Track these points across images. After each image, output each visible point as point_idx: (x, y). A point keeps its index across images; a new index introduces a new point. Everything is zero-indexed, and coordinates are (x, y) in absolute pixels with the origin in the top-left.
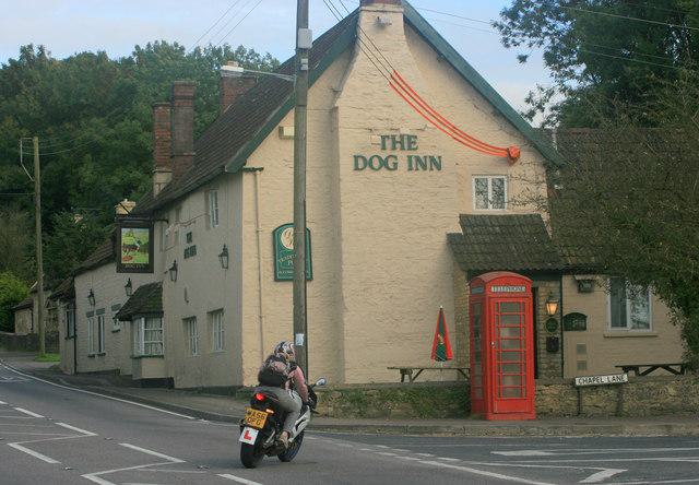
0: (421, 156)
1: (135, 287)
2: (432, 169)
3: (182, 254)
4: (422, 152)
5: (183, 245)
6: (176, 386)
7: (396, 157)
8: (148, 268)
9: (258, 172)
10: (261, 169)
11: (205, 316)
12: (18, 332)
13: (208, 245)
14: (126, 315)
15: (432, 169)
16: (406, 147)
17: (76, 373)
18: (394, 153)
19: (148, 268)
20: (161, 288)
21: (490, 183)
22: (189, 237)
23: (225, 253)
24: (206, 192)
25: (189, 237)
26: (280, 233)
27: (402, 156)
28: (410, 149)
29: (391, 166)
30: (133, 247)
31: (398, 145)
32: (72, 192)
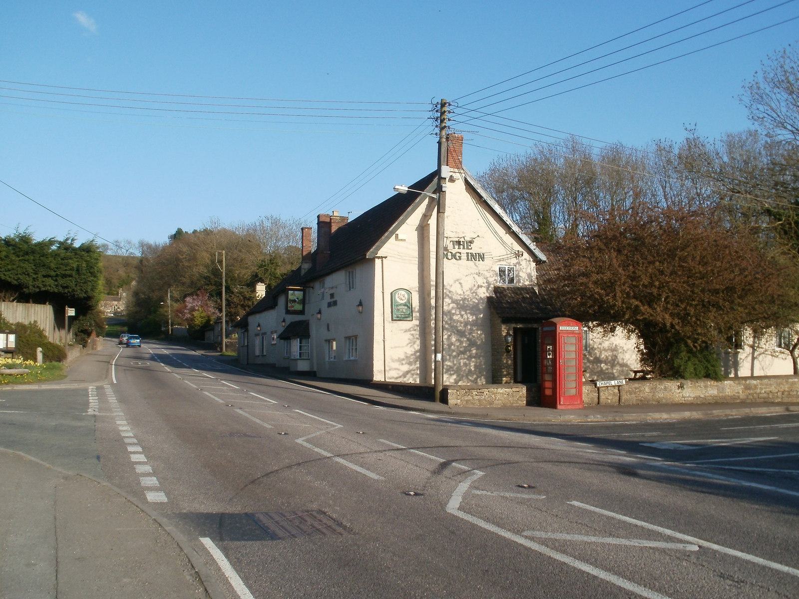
0: (474, 253)
1: (288, 322)
2: (479, 261)
3: (327, 305)
4: (475, 249)
5: (328, 299)
6: (318, 375)
7: (460, 253)
8: (302, 312)
9: (384, 259)
10: (386, 257)
11: (343, 340)
12: (206, 341)
13: (348, 301)
14: (286, 336)
15: (479, 261)
16: (466, 248)
17: (248, 364)
18: (459, 251)
19: (302, 312)
20: (308, 323)
21: (507, 269)
22: (332, 296)
23: (361, 304)
24: (777, 326)
25: (332, 296)
26: (395, 294)
27: (464, 252)
28: (468, 248)
29: (458, 258)
30: (294, 301)
31: (462, 247)
32: (639, 359)
